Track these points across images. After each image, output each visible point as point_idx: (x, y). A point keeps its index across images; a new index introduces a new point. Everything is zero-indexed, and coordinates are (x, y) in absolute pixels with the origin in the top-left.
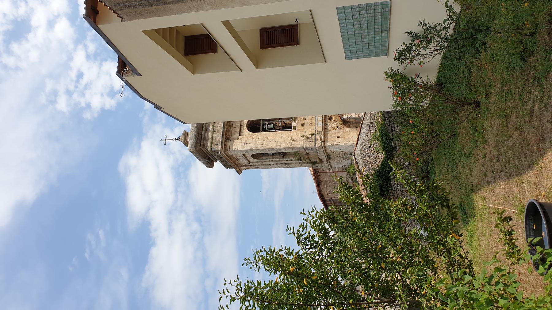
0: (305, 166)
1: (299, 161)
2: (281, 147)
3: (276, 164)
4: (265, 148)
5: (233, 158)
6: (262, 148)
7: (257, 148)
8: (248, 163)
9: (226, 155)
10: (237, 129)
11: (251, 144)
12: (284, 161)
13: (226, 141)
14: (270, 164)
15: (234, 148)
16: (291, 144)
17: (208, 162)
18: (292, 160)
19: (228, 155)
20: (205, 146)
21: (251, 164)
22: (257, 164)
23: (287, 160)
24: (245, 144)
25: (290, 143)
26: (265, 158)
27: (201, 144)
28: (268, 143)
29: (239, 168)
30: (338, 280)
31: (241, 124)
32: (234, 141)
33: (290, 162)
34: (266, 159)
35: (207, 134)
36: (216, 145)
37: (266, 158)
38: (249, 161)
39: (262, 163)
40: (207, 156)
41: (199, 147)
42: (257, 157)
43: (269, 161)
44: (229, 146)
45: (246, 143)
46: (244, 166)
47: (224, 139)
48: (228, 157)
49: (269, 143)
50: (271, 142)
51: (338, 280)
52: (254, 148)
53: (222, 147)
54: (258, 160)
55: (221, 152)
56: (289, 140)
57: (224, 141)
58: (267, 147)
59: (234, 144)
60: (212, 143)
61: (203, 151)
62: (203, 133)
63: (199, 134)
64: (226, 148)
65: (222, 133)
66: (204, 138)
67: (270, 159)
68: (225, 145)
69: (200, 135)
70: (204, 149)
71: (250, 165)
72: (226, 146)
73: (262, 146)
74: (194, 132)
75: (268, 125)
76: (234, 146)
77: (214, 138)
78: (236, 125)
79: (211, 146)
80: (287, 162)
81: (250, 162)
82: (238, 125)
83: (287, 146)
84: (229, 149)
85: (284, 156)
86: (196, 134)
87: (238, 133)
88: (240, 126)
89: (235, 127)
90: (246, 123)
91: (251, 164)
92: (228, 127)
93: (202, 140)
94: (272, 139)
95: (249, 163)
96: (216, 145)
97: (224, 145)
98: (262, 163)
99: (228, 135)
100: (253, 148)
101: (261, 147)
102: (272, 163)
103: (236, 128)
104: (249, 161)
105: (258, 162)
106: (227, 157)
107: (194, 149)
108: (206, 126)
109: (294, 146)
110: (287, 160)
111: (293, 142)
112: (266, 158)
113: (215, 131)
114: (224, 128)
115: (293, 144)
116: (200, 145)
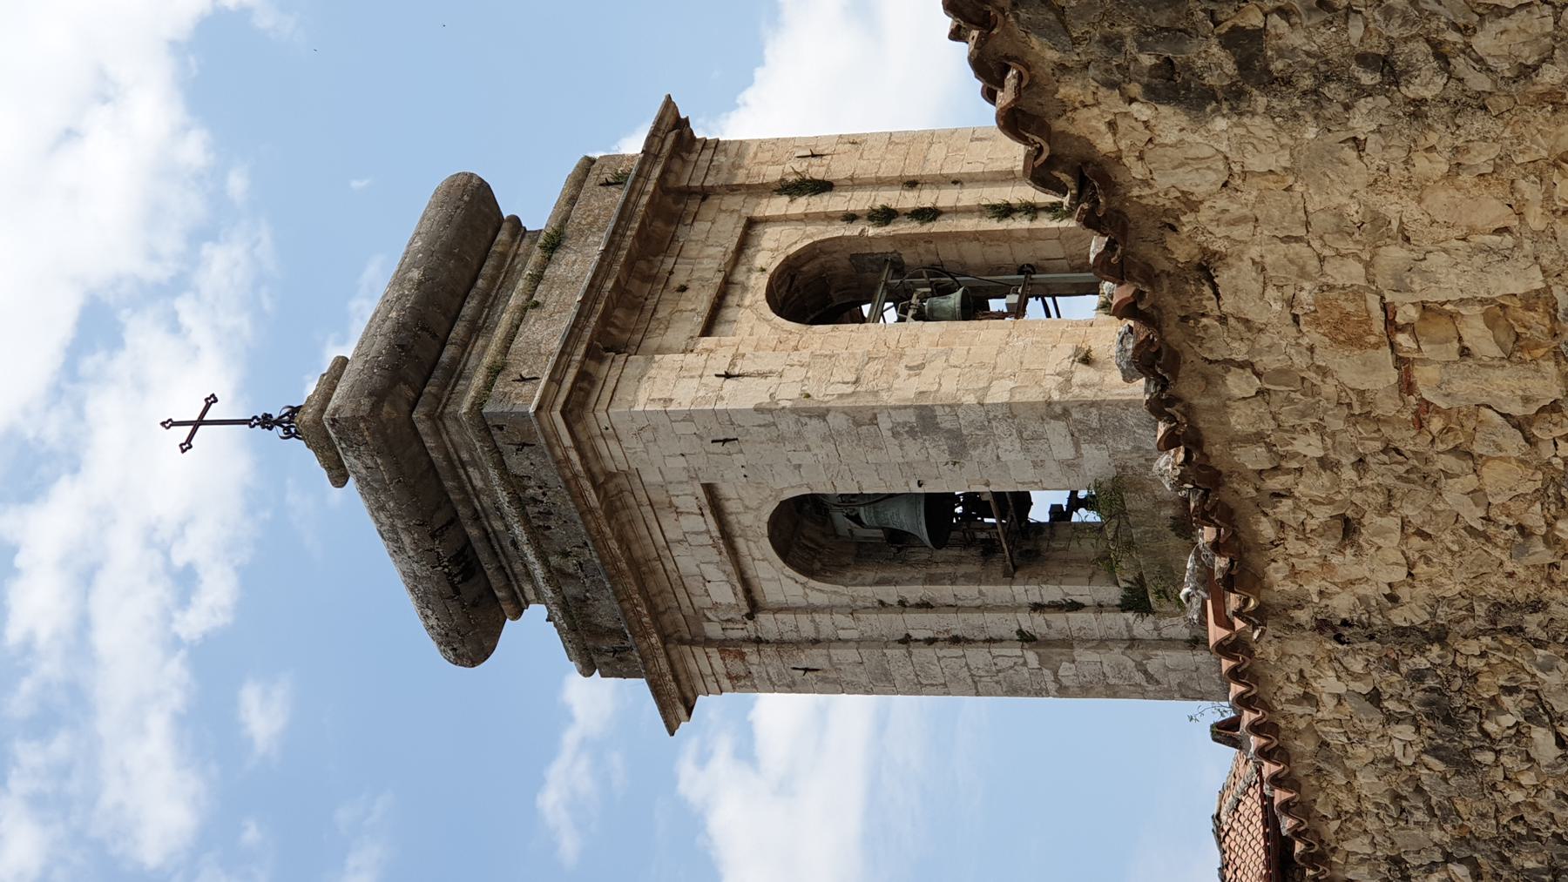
0: (1174, 679)
1: (1130, 616)
2: (988, 401)
3: (956, 640)
4: (870, 401)
5: (631, 521)
6: (848, 402)
7: (809, 403)
8: (746, 610)
9: (574, 456)
10: (700, 302)
11: (773, 380)
12: (1016, 608)
13: (594, 354)
14: (906, 640)
15: (642, 397)
16: (1069, 381)
17: (457, 592)
18: (1075, 606)
19: (596, 469)
20: (450, 409)
21: (768, 624)
22: (806, 625)
23: (1037, 607)
24: (728, 376)
25: (1061, 379)
26: (870, 575)
27: (420, 395)
28: (897, 376)
29: (674, 654)
30: (990, 301)
31: (731, 273)
32: (657, 357)
33: (1059, 620)
34: (879, 583)
35: (480, 342)
36: (523, 379)
37: (880, 575)
38: (748, 590)
39: (847, 626)
40: (454, 520)
41: (405, 408)
42: (817, 565)
43: (902, 603)
44: (611, 384)
45: (736, 371)
46: (708, 642)
47: (587, 333)
48: (592, 478)
49: (904, 373)
50: (921, 366)
51: (990, 301)
52: (788, 404)
53: (560, 383)
54: (819, 592)
55: (539, 408)
56: (1062, 357)
57: (582, 349)
58: (888, 399)
59: (652, 372)
60: (496, 371)
61: (431, 462)
62: (459, 329)
63: (422, 329)
64: (588, 394)
65: (579, 298)
66: (455, 361)
67: (911, 581)
68: (584, 376)
69: (434, 336)
70: (437, 433)
71: (758, 641)
72: (593, 383)
73: (849, 389)
74: (394, 314)
75: (923, 298)
76: (645, 385)
77: (519, 342)
78: (696, 275)
79: (489, 385)
80: (1035, 623)
81: (754, 608)
82: (708, 275)
83: (1033, 395)
84: (602, 406)
85: (1016, 568)
86: (401, 327)
87: (699, 321)
88: (719, 279)
89: (683, 289)
90: (771, 269)
91: (768, 624)
92: (635, 286)
93: (438, 373)
94: (933, 350)
95: (750, 616)
96: (523, 379)
97: (571, 374)
98: (847, 626)
99: (623, 331)
100: (783, 404)
101: (841, 396)
102: (921, 624)
103: (689, 293)
104: (748, 590)
105: (812, 609)
106: (587, 484)
107: (367, 408)
108: (489, 295)
109: (1089, 394)
110: (1037, 607)
111: (1083, 374)
112: (880, 575)
113: (536, 305)
114: (607, 276)
115: (1084, 386)
116: (417, 400)
